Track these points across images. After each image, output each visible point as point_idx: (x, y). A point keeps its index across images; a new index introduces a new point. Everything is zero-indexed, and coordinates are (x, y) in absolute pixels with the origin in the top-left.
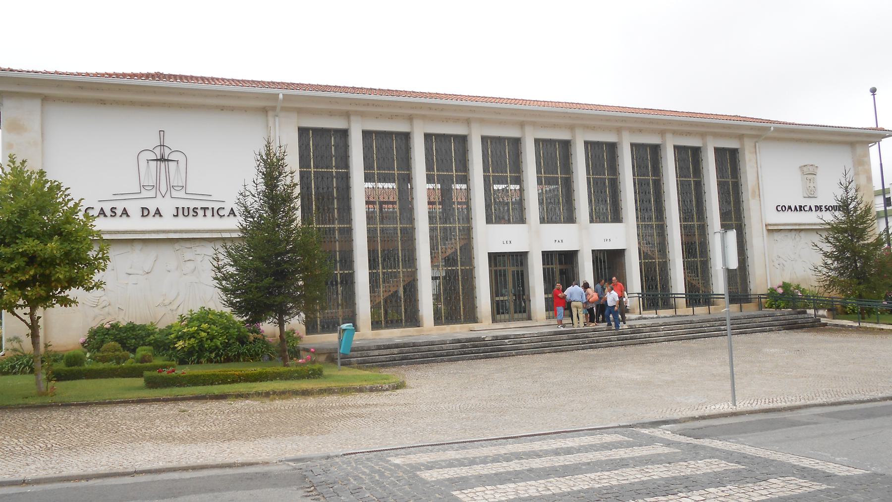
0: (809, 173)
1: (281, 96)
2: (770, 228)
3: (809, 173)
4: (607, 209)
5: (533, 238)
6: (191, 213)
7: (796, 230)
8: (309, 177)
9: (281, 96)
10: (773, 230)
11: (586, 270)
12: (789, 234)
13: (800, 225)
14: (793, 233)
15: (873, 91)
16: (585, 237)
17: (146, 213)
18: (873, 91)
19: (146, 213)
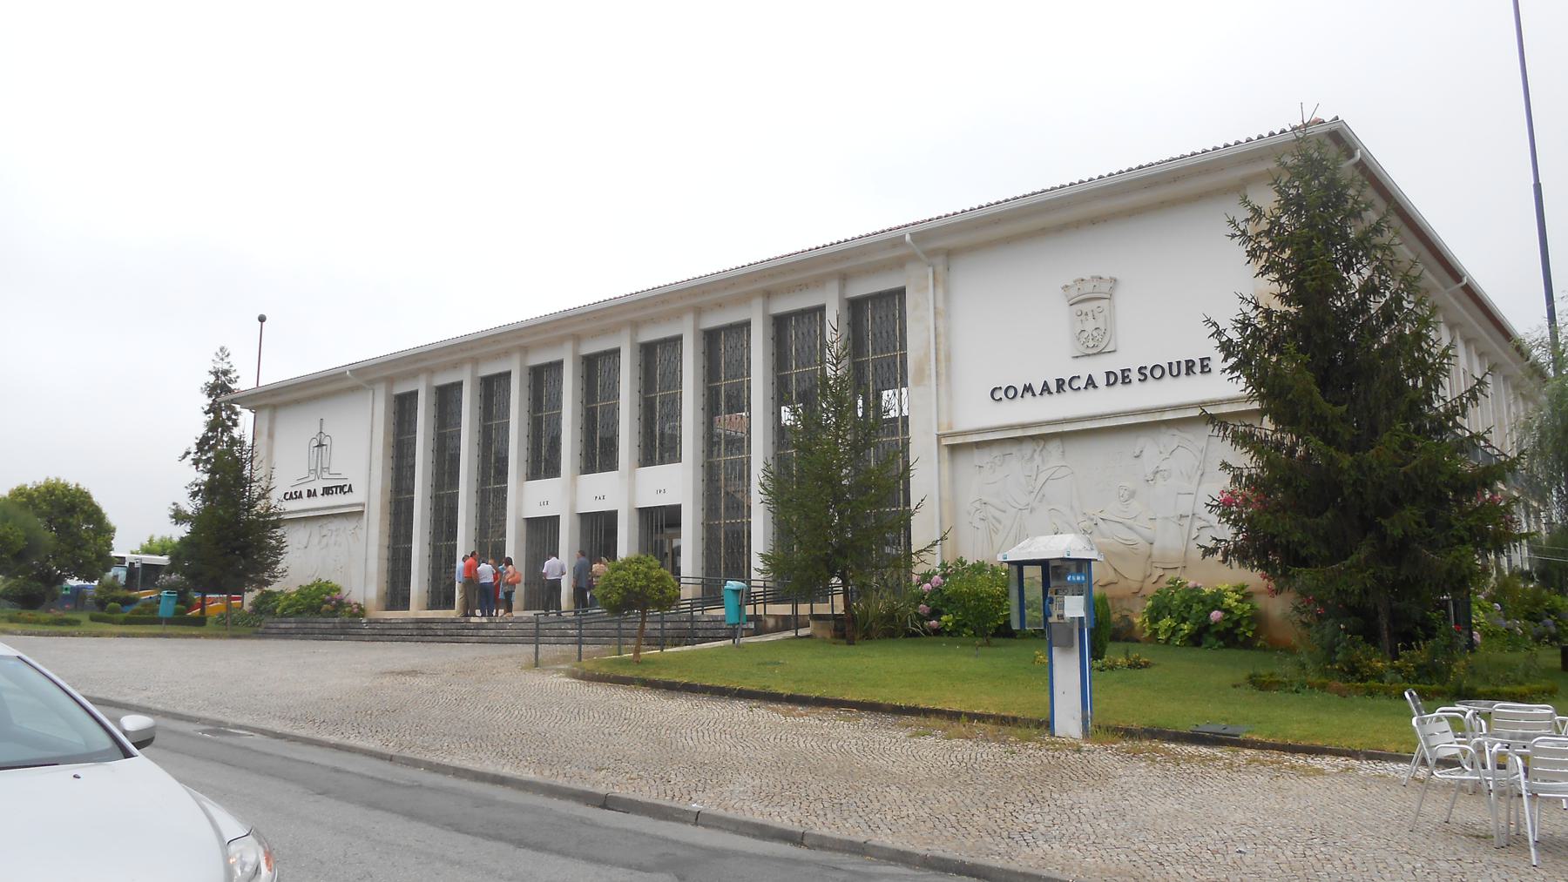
0: (1091, 298)
1: (908, 238)
2: (950, 441)
3: (1091, 298)
4: (658, 447)
5: (627, 489)
6: (1148, 372)
7: (1032, 438)
8: (718, 393)
9: (908, 238)
10: (957, 448)
11: (568, 538)
12: (1014, 450)
13: (1024, 426)
14: (1027, 449)
15: (262, 319)
16: (627, 489)
17: (1112, 379)
18: (262, 319)
19: (1112, 379)
